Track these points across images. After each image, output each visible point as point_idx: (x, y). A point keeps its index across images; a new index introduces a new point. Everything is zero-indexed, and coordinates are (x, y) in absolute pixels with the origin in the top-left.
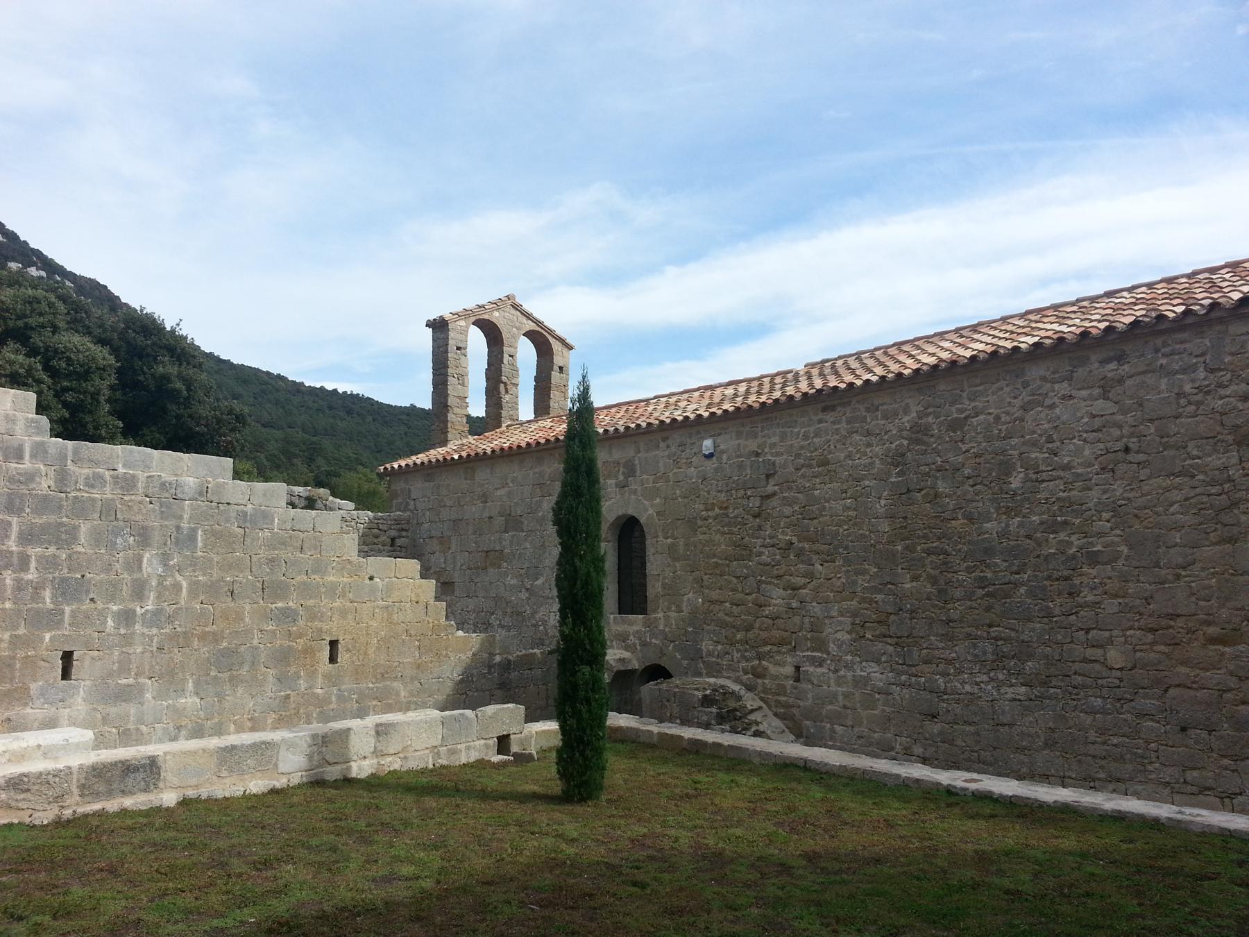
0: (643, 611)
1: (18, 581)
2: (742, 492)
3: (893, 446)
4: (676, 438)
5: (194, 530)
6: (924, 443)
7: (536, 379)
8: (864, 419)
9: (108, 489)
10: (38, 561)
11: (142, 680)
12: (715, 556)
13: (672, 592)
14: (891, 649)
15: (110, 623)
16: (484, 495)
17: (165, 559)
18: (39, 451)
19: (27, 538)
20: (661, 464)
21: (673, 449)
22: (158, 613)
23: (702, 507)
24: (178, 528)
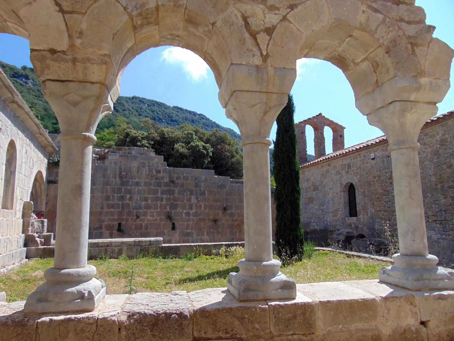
0: (356, 216)
1: (161, 204)
2: (385, 171)
3: (434, 148)
4: (362, 153)
5: (205, 190)
6: (446, 145)
7: (333, 140)
8: (423, 139)
9: (182, 180)
10: (166, 200)
11: (193, 231)
12: (377, 195)
13: (365, 208)
14: (439, 225)
15: (184, 216)
16: (308, 179)
17: (197, 198)
18: (165, 171)
19: (163, 193)
20: (358, 164)
21: (362, 158)
22: (196, 213)
23: (372, 177)
24: (200, 190)
